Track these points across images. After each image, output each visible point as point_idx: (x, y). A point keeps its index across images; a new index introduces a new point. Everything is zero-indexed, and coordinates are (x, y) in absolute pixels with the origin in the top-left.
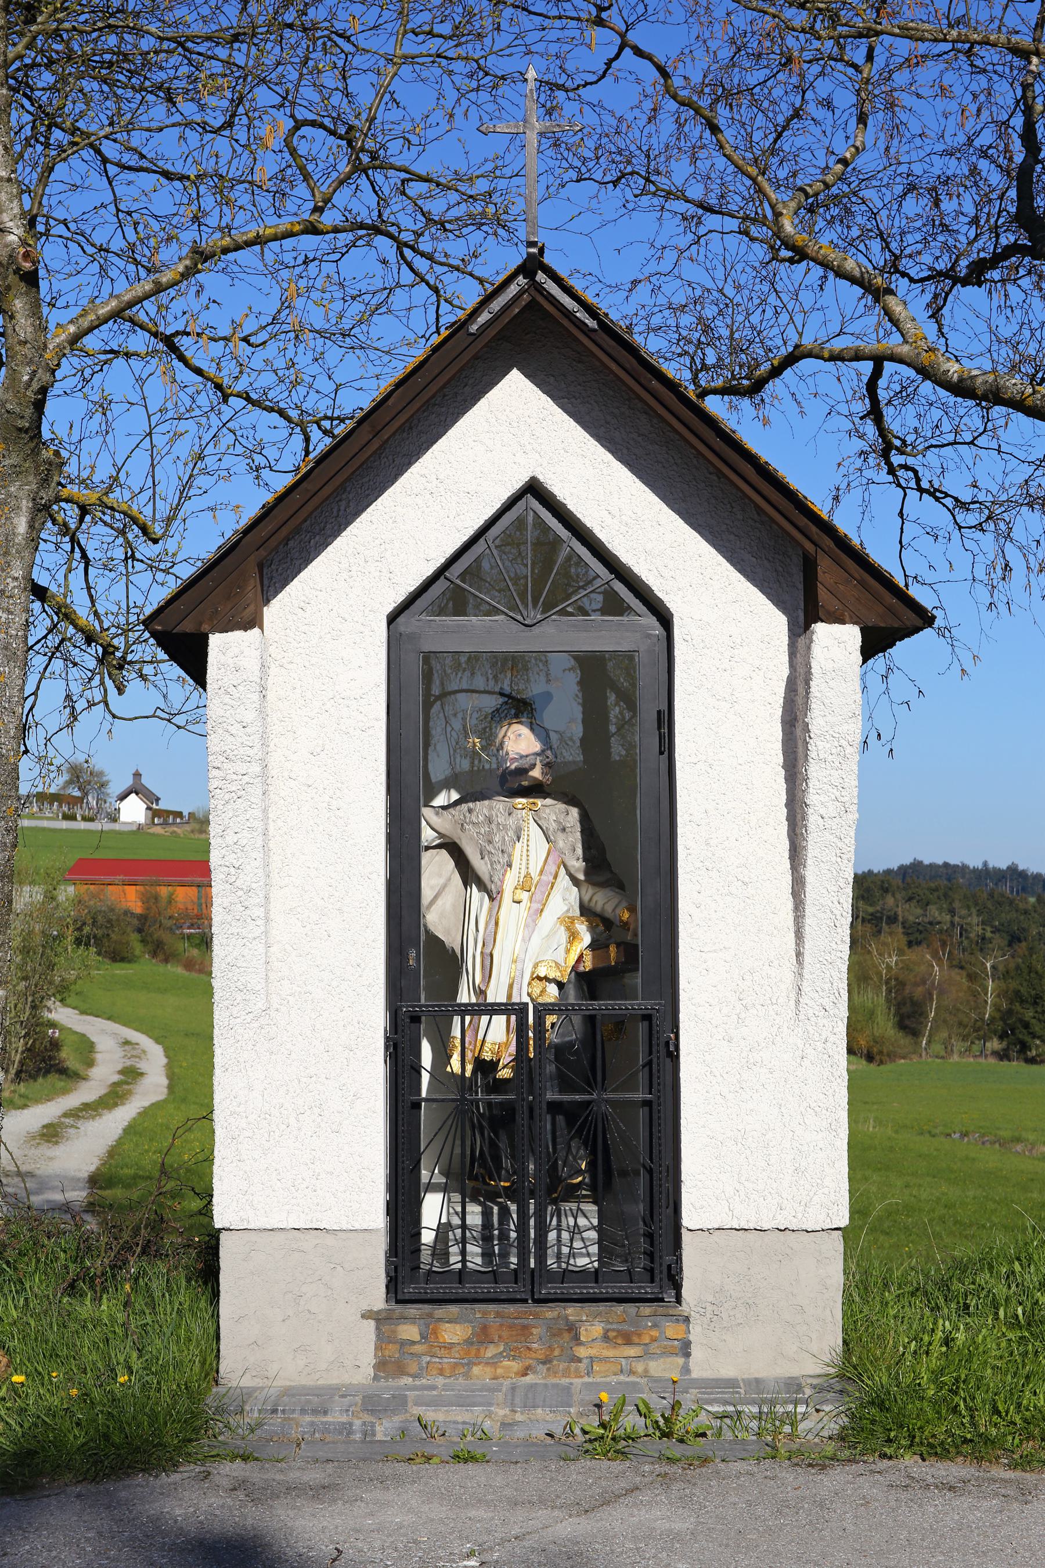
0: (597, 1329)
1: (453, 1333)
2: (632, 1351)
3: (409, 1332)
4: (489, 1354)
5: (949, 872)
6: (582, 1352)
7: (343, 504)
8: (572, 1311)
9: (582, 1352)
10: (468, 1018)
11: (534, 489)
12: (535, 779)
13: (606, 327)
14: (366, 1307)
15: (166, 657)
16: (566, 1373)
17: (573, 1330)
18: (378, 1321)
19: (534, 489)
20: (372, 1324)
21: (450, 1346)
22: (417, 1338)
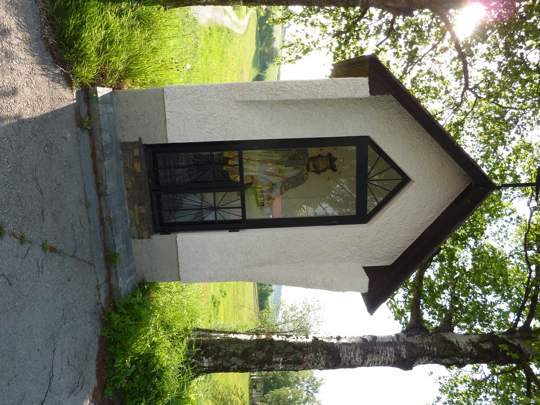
0: (143, 211)
1: (137, 167)
2: (138, 222)
3: (136, 152)
4: (132, 178)
5: (293, 286)
6: (136, 207)
7: (408, 120)
8: (148, 204)
9: (136, 207)
10: (238, 167)
11: (405, 180)
12: (96, 93)
13: (149, 177)
14: (143, 138)
15: (328, 205)
16: (129, 203)
17: (141, 204)
18: (138, 142)
19: (405, 180)
20: (138, 140)
21: (133, 165)
22: (135, 155)
